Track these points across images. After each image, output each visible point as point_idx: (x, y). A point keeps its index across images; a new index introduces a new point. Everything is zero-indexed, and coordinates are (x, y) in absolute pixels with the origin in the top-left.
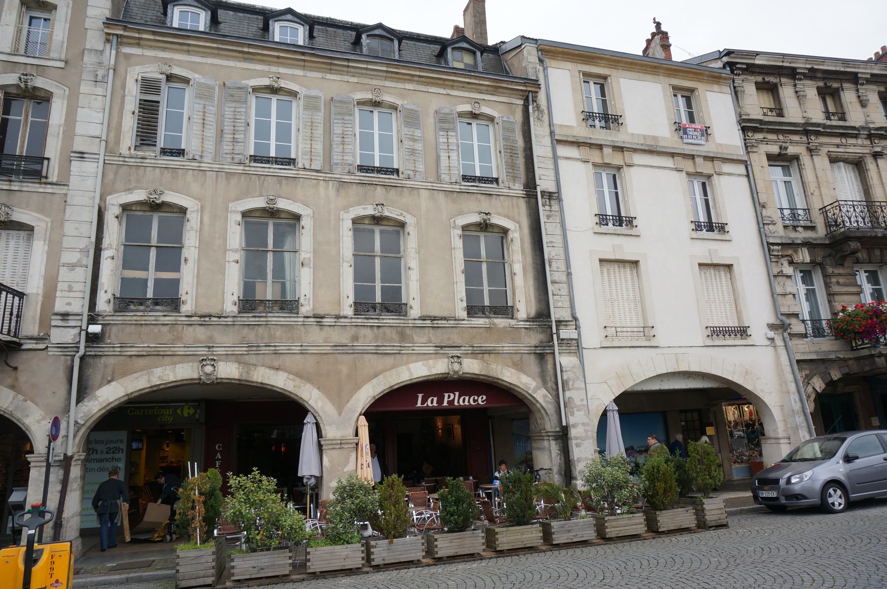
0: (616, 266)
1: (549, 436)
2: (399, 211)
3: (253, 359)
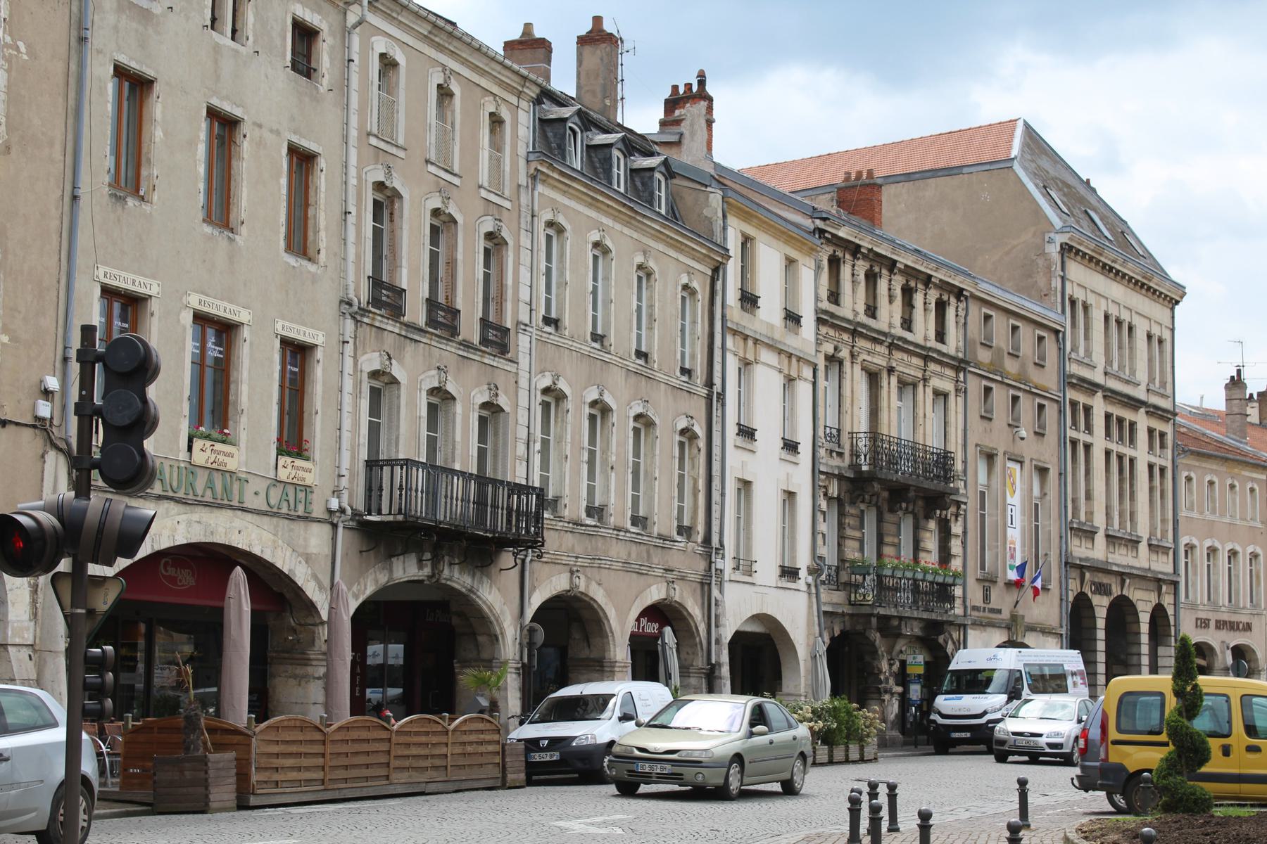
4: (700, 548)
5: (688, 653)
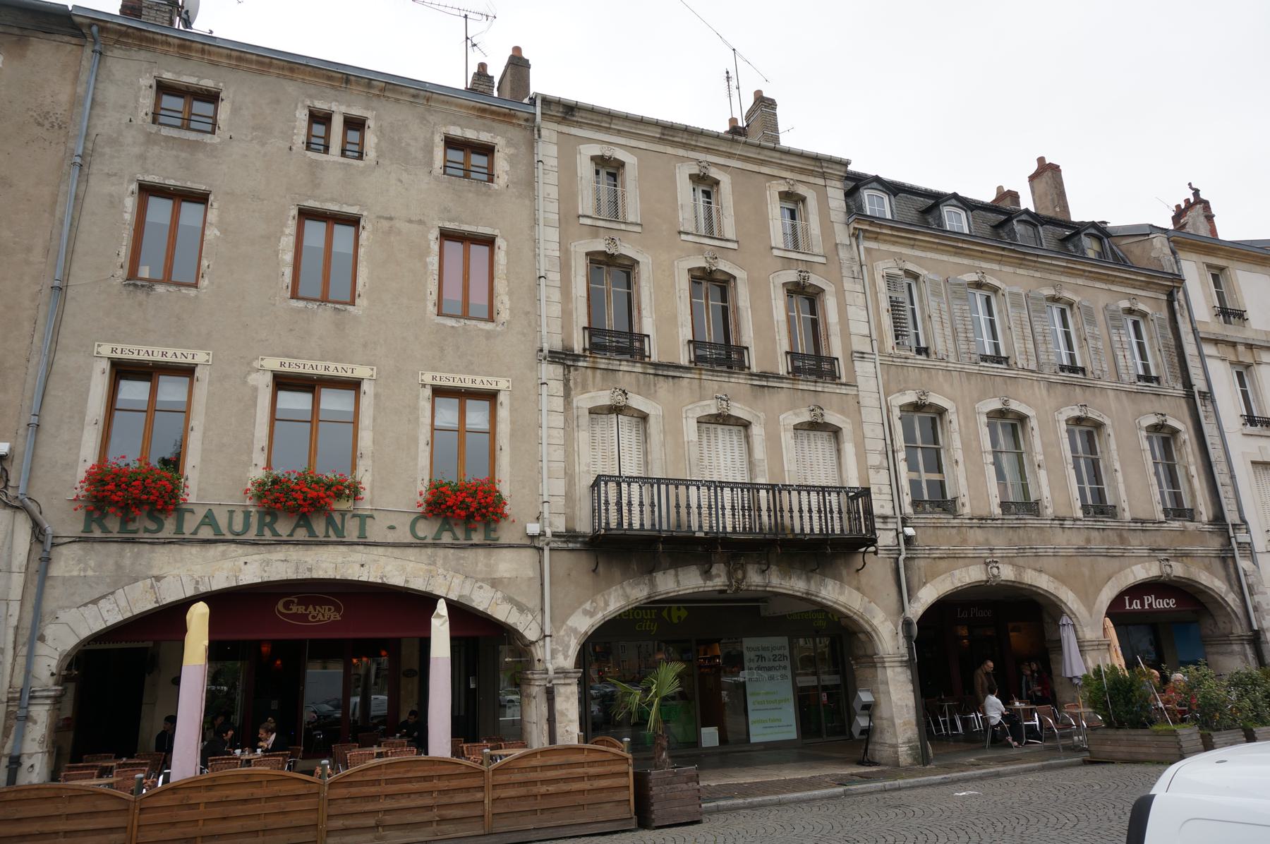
1: (1243, 640)
2: (1098, 413)
4: (1206, 526)
5: (1224, 622)
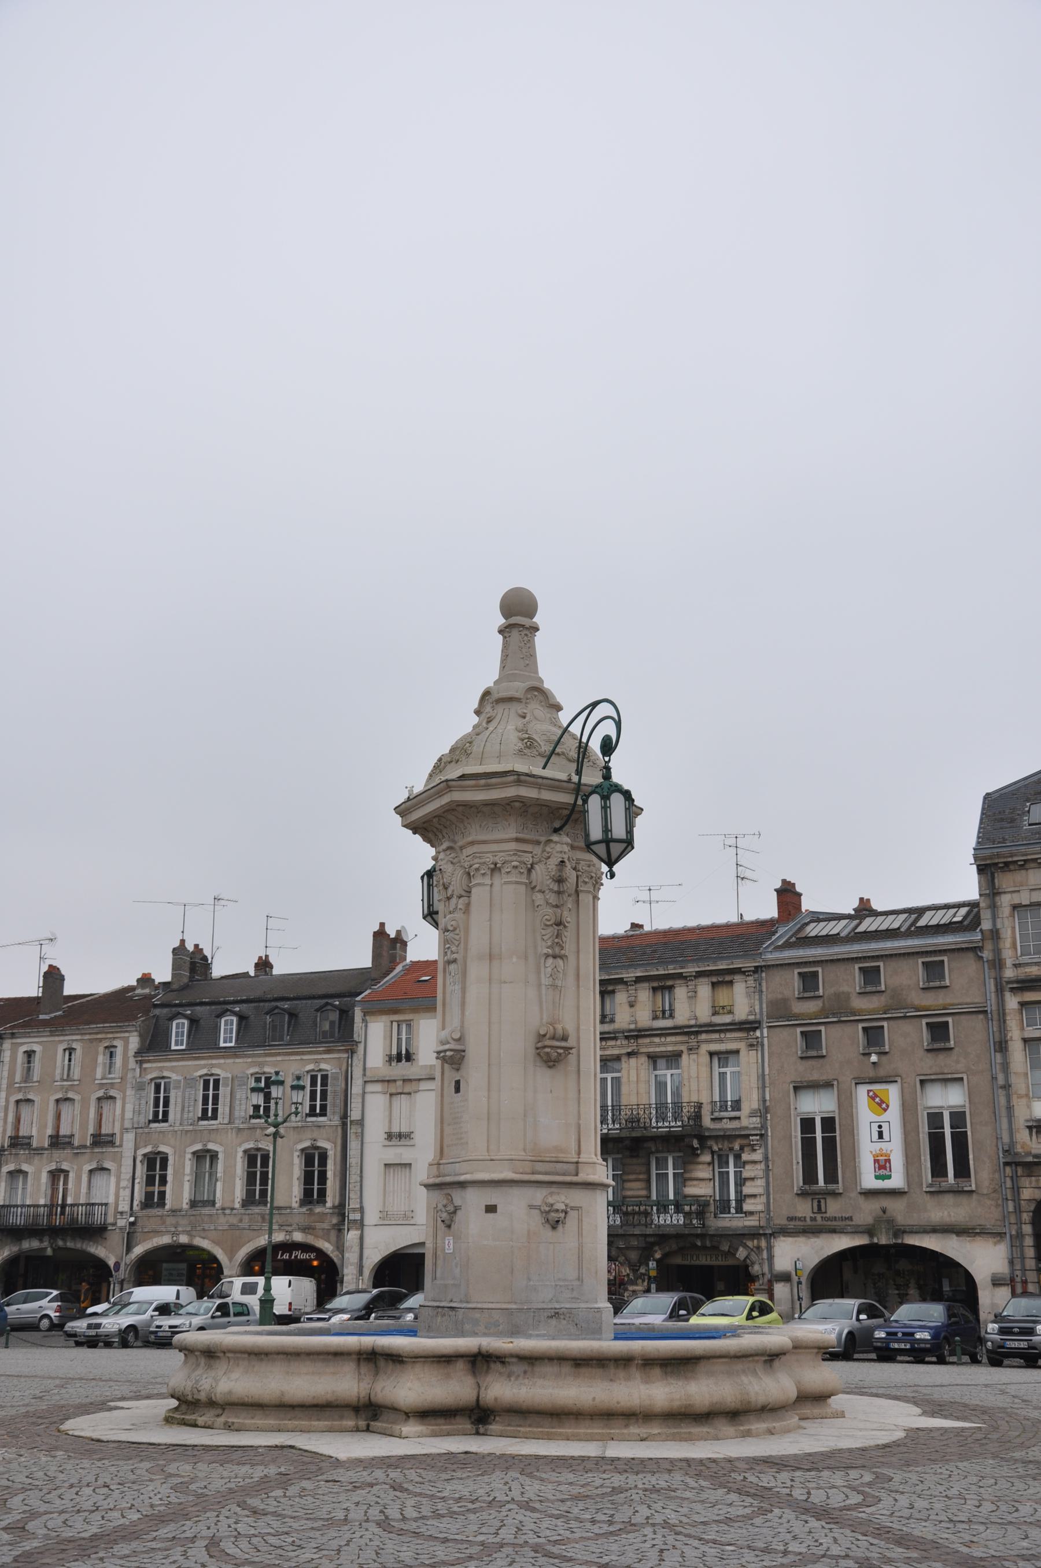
0: (399, 1167)
3: (194, 1233)
